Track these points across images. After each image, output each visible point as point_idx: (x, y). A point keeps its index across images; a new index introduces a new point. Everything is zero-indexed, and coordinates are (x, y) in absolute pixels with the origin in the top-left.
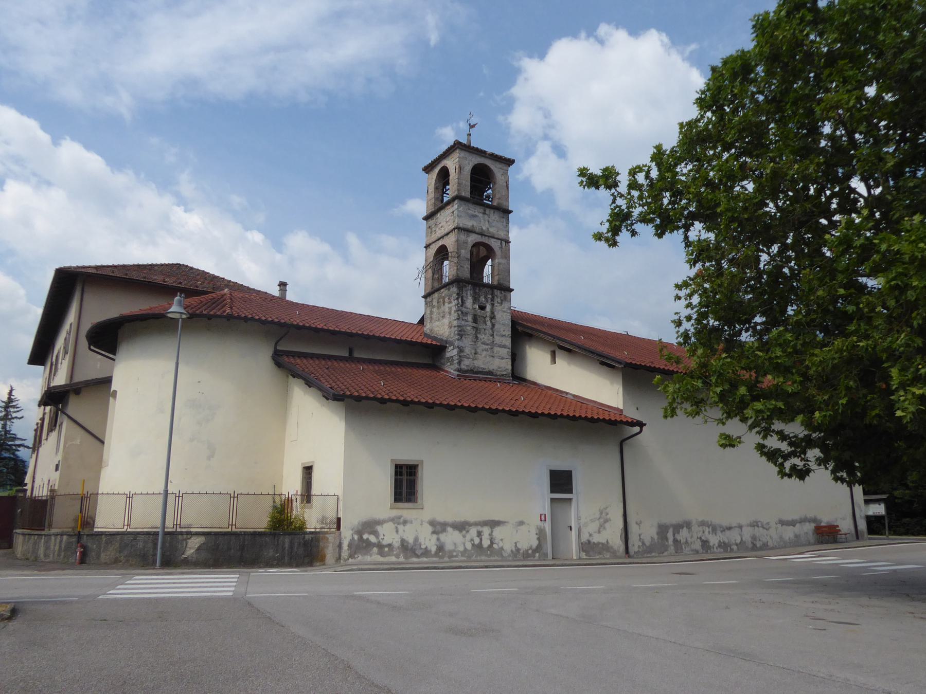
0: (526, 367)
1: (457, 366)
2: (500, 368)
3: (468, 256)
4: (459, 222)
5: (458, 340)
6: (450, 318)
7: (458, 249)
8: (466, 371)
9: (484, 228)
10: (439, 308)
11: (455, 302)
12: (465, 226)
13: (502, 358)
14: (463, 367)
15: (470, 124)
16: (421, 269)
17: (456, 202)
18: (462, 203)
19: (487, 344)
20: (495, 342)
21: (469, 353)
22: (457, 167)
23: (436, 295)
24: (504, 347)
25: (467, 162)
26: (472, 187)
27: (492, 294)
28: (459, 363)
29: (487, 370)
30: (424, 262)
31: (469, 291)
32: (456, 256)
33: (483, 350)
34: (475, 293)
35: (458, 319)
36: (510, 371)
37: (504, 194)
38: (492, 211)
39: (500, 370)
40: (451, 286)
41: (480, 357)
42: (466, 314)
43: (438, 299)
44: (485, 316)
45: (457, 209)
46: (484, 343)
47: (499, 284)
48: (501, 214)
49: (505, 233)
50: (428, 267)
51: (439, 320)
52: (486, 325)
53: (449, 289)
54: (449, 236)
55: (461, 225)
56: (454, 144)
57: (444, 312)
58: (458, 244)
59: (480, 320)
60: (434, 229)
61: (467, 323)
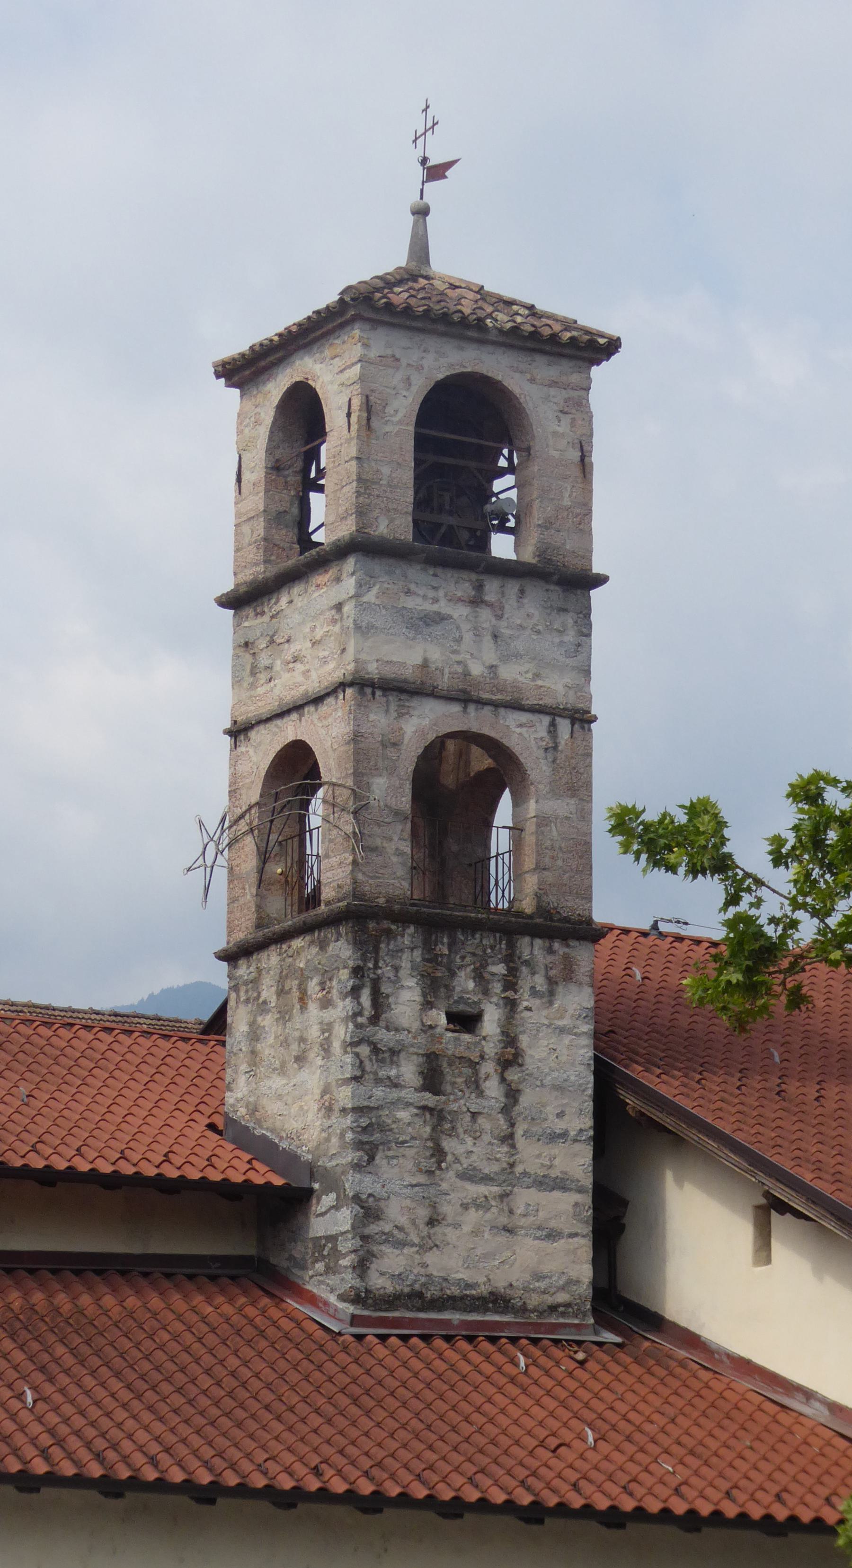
0: (663, 1260)
1: (348, 1280)
2: (539, 1277)
3: (405, 802)
4: (363, 656)
5: (357, 1167)
6: (325, 1069)
7: (357, 775)
8: (392, 1301)
9: (476, 669)
10: (284, 1016)
11: (343, 1007)
12: (389, 672)
13: (553, 1235)
14: (379, 1282)
15: (424, 161)
16: (212, 825)
17: (350, 564)
18: (377, 566)
19: (486, 1179)
20: (519, 1169)
21: (403, 1220)
22: (356, 403)
23: (271, 959)
24: (560, 1184)
25: (399, 376)
26: (421, 504)
27: (510, 959)
28: (362, 1267)
29: (484, 1290)
30: (223, 801)
31: (406, 956)
32: (351, 806)
33: (465, 1207)
34: (432, 959)
35: (356, 1079)
36: (585, 1289)
37: (567, 502)
38: (513, 587)
39: (542, 1285)
40: (329, 933)
41: (451, 1234)
42: (394, 1053)
43: (281, 979)
44: (475, 1057)
45: (357, 596)
46: (470, 1176)
47: (543, 910)
48: (556, 594)
49: (569, 678)
50: (243, 826)
51: (282, 1070)
52: (481, 1094)
53: (323, 946)
54: (324, 708)
55: (373, 670)
56: (341, 301)
57: (302, 1040)
58: (357, 752)
59: (455, 1077)
60: (264, 660)
61: (395, 1094)
